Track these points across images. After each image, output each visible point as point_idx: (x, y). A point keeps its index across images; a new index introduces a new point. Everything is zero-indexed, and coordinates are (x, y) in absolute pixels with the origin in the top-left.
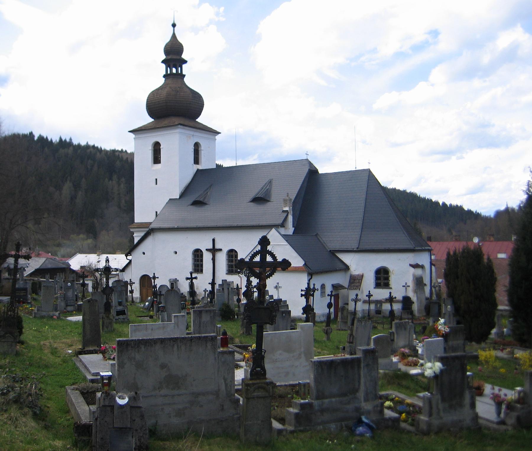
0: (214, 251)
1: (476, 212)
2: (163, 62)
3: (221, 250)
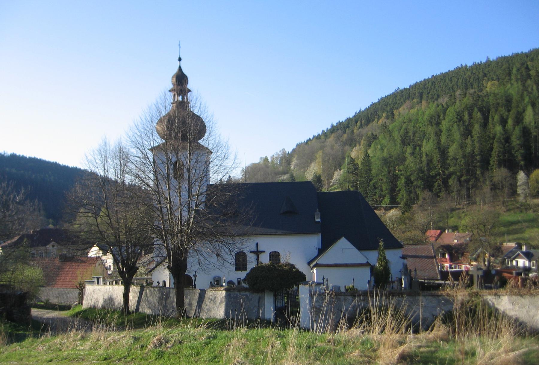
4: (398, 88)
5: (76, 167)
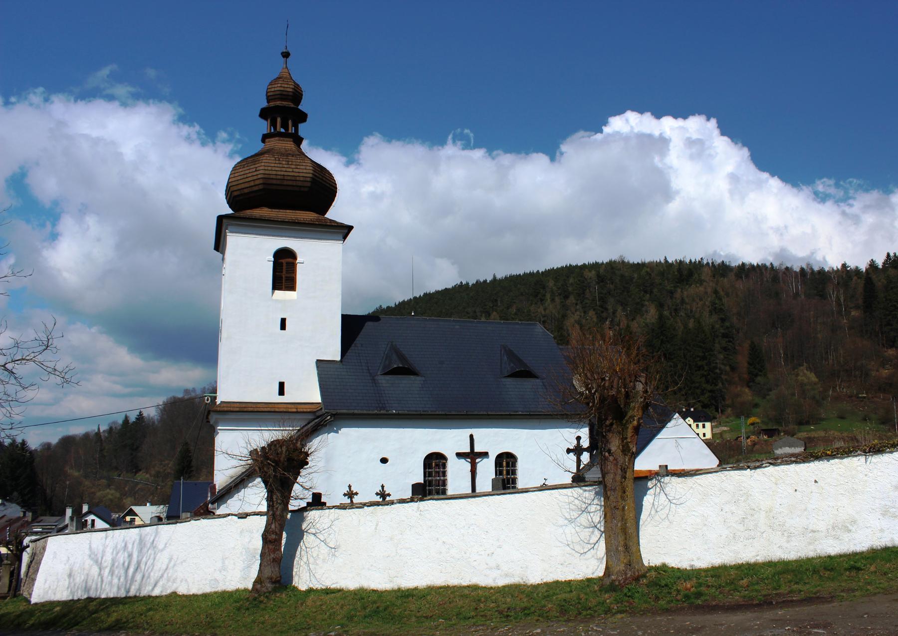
3: (485, 455)
4: (381, 306)
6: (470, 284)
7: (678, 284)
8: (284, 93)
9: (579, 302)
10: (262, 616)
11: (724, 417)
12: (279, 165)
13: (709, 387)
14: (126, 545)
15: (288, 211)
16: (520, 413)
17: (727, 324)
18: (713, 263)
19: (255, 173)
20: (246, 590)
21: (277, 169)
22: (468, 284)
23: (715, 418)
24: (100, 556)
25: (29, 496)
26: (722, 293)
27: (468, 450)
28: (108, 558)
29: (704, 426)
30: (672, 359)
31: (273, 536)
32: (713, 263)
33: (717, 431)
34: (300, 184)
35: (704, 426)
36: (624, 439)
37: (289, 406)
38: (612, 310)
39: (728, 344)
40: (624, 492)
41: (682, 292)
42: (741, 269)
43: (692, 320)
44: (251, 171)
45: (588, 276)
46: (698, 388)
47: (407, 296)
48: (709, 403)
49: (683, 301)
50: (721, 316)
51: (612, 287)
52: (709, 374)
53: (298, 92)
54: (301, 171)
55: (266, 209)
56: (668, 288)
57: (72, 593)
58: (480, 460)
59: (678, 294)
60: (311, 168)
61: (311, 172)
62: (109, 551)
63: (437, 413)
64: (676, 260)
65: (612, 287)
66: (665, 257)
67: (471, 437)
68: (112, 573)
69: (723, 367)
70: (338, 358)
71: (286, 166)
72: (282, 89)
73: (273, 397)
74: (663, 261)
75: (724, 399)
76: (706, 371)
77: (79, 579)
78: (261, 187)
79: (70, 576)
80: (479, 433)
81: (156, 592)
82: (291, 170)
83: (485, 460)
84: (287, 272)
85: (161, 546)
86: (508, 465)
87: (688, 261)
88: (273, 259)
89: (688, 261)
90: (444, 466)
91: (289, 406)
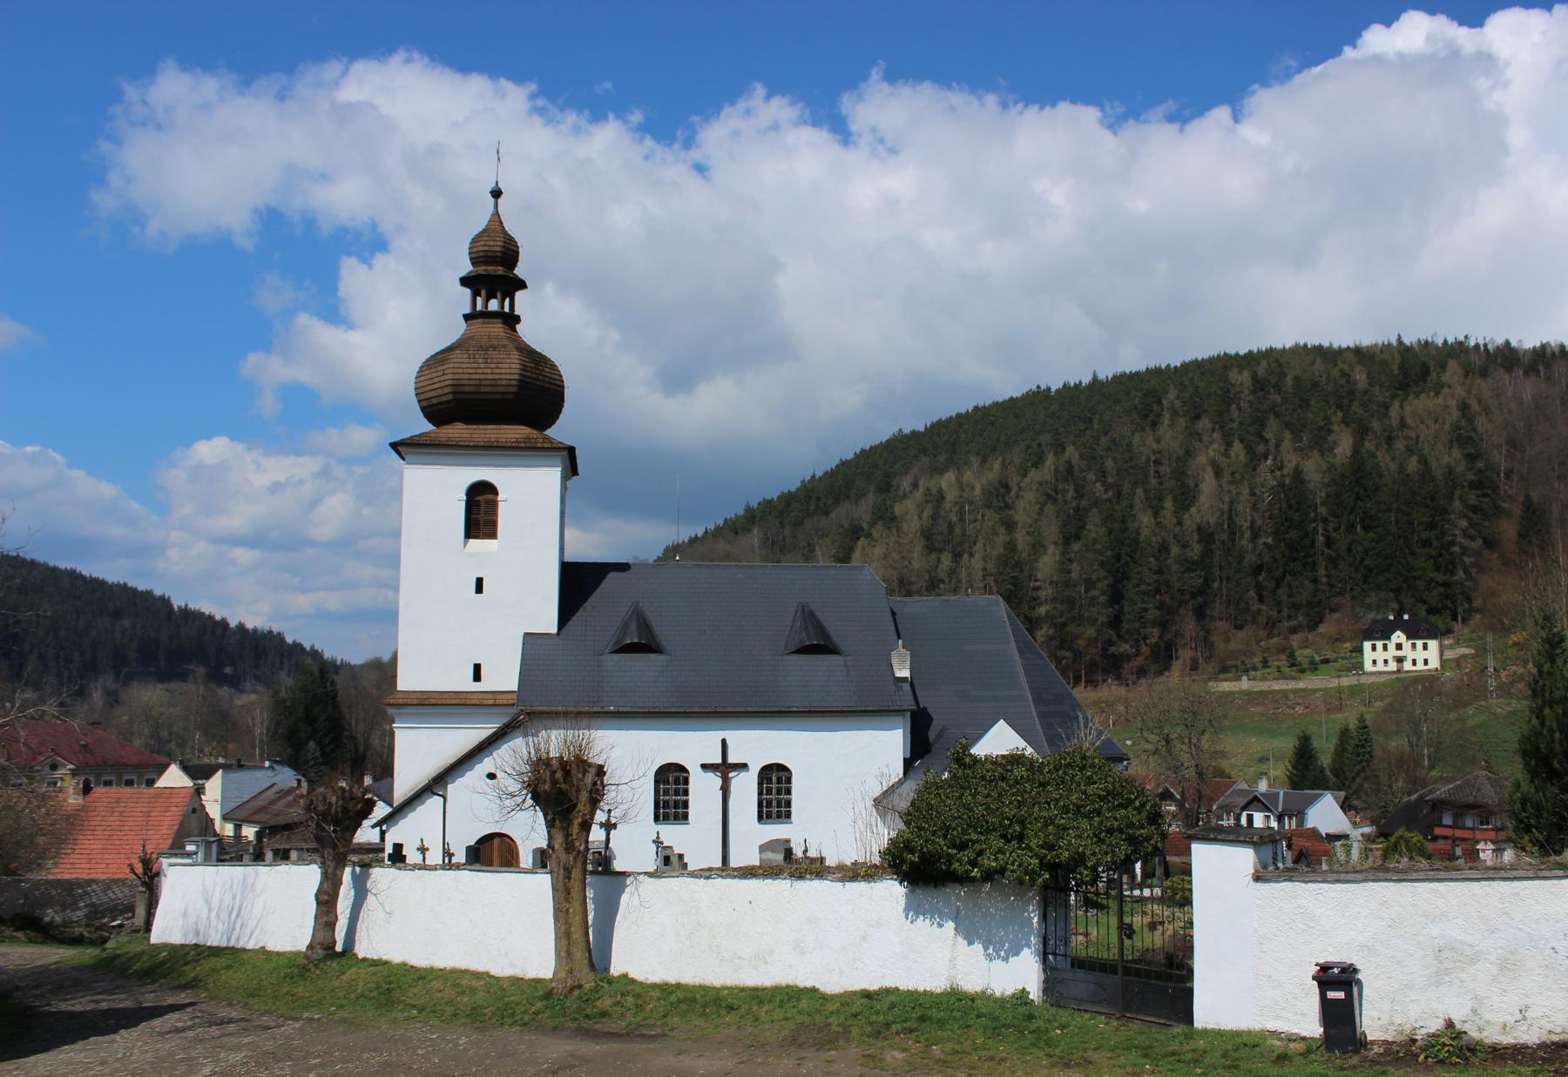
0: (725, 769)
1: (312, 648)
2: (465, 281)
3: (743, 767)
4: (900, 430)
5: (125, 584)
6: (1053, 390)
7: (1399, 392)
8: (491, 254)
9: (1217, 427)
10: (297, 987)
11: (1466, 630)
12: (473, 365)
13: (1440, 577)
14: (232, 885)
15: (490, 427)
16: (795, 709)
17: (1481, 465)
18: (1485, 345)
19: (442, 378)
20: (298, 953)
21: (470, 371)
22: (1049, 389)
23: (1449, 631)
24: (210, 894)
25: (332, 746)
26: (1475, 407)
27: (720, 761)
28: (217, 898)
29: (1425, 647)
30: (1376, 527)
31: (326, 898)
32: (1485, 345)
33: (1449, 654)
34: (502, 389)
35: (1425, 647)
36: (567, 836)
37: (486, 696)
38: (1274, 441)
39: (1482, 499)
40: (569, 894)
41: (1402, 407)
42: (1538, 355)
43: (1415, 459)
44: (438, 374)
45: (1237, 380)
46: (1419, 578)
47: (1005, 385)
48: (1440, 605)
49: (1403, 424)
50: (1469, 451)
51: (1278, 398)
52: (1440, 555)
53: (509, 249)
54: (503, 371)
55: (460, 426)
56: (1381, 399)
57: (185, 936)
58: (735, 773)
59: (1394, 412)
60: (518, 366)
61: (518, 371)
62: (218, 889)
63: (673, 710)
64: (1419, 341)
65: (1278, 398)
66: (1399, 335)
67: (724, 742)
68: (218, 916)
69: (1466, 542)
70: (554, 630)
71: (482, 366)
72: (486, 248)
73: (467, 684)
74: (1394, 342)
75: (1469, 599)
76: (1435, 549)
77: (192, 919)
78: (450, 397)
79: (185, 914)
80: (733, 736)
81: (250, 946)
82: (489, 371)
83: (743, 774)
84: (487, 513)
85: (258, 891)
86: (779, 781)
87: (1440, 342)
88: (465, 498)
89: (1440, 342)
90: (686, 781)
91: (486, 696)
